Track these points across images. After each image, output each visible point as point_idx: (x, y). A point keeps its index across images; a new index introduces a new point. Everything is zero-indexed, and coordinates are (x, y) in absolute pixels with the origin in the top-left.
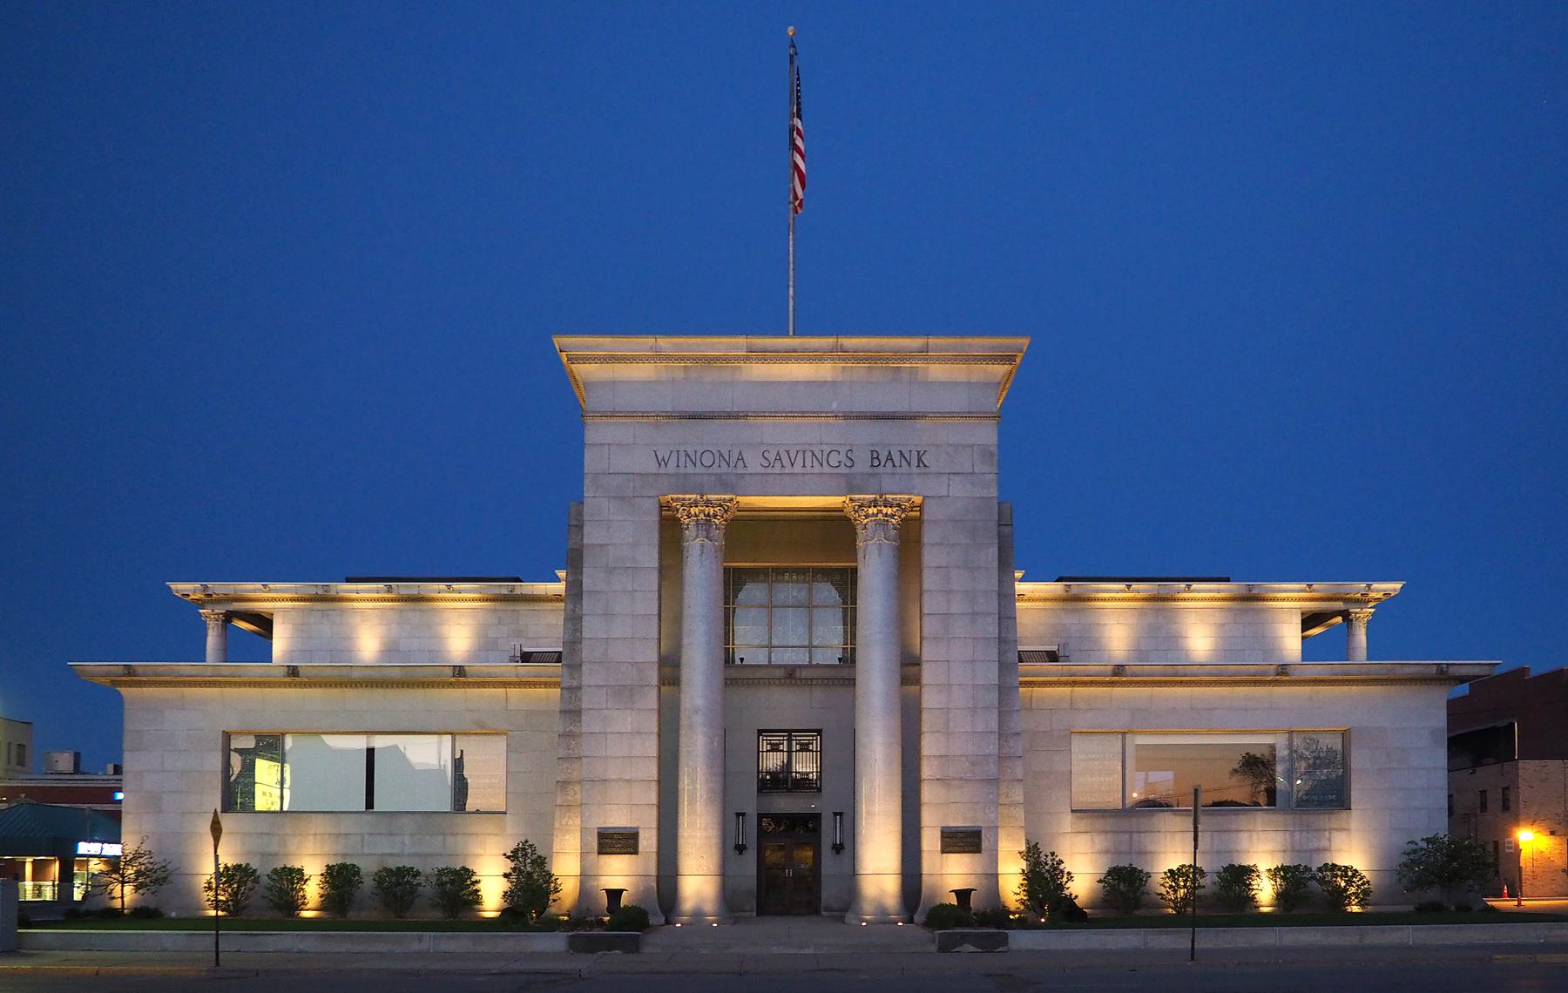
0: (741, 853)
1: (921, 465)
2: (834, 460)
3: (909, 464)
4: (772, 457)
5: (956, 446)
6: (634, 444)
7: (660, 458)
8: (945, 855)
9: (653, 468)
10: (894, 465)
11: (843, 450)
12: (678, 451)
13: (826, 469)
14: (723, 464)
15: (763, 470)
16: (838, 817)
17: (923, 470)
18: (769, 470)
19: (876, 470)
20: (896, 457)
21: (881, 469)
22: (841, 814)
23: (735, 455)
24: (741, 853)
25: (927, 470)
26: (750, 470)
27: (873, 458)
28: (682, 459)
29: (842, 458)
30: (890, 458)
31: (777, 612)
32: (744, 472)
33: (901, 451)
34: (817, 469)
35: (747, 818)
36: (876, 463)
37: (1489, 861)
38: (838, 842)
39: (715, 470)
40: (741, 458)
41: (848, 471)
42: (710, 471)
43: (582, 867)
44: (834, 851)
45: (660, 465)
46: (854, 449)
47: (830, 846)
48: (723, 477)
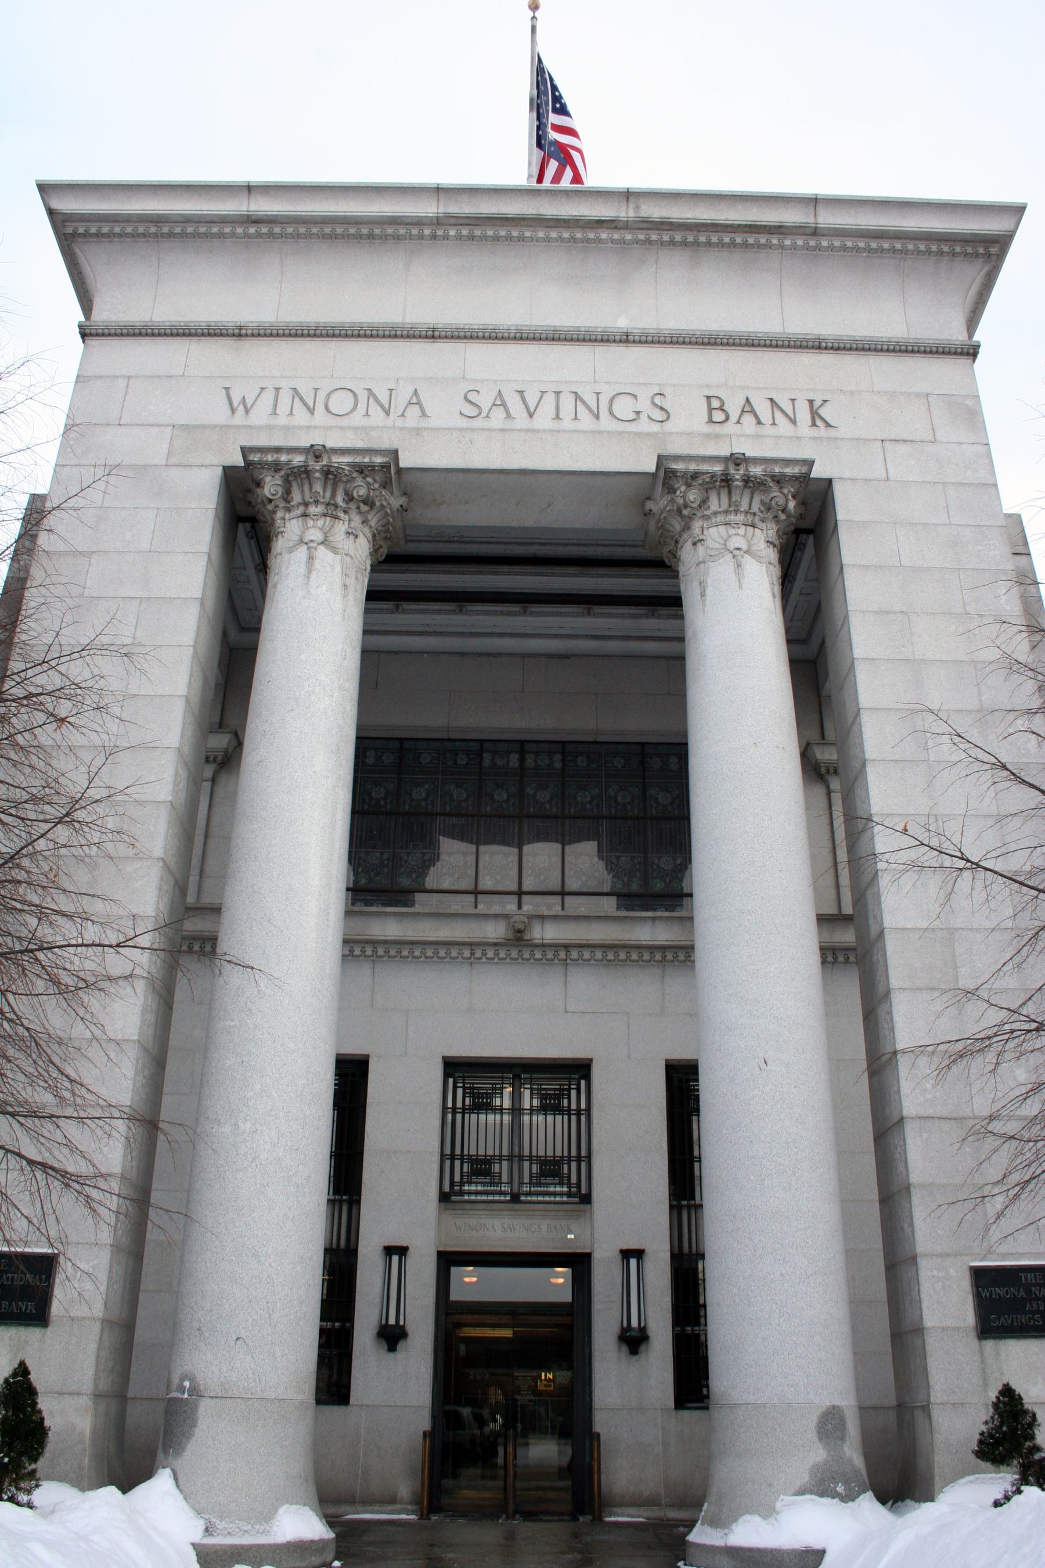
0: (392, 1347)
1: (819, 422)
2: (624, 408)
3: (793, 422)
4: (485, 400)
5: (892, 395)
6: (183, 375)
7: (236, 401)
8: (989, 1344)
9: (220, 415)
10: (759, 423)
11: (644, 396)
12: (278, 389)
13: (606, 423)
14: (376, 411)
15: (464, 423)
16: (633, 1262)
17: (822, 431)
18: (478, 423)
19: (717, 429)
20: (764, 410)
21: (730, 428)
22: (639, 1254)
23: (404, 394)
24: (392, 1347)
25: (832, 433)
26: (432, 423)
27: (710, 409)
28: (285, 397)
29: (644, 404)
30: (748, 408)
31: (525, 898)
32: (423, 425)
33: (771, 400)
34: (586, 420)
35: (411, 1259)
36: (718, 416)
37: (500, 1398)
38: (634, 1323)
39: (357, 419)
40: (416, 400)
41: (656, 428)
42: (345, 422)
43: (898, 1398)
44: (625, 1348)
45: (233, 411)
46: (668, 391)
47: (615, 1329)
48: (374, 433)
